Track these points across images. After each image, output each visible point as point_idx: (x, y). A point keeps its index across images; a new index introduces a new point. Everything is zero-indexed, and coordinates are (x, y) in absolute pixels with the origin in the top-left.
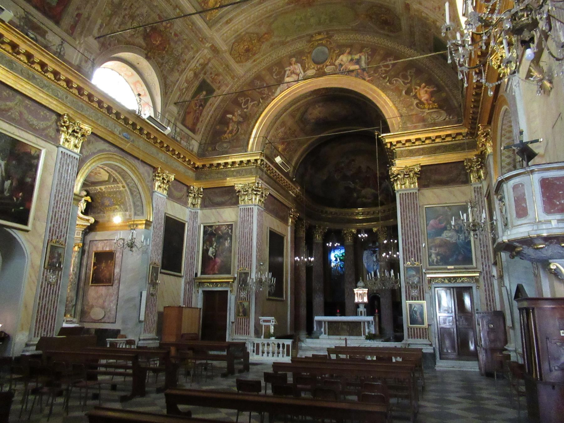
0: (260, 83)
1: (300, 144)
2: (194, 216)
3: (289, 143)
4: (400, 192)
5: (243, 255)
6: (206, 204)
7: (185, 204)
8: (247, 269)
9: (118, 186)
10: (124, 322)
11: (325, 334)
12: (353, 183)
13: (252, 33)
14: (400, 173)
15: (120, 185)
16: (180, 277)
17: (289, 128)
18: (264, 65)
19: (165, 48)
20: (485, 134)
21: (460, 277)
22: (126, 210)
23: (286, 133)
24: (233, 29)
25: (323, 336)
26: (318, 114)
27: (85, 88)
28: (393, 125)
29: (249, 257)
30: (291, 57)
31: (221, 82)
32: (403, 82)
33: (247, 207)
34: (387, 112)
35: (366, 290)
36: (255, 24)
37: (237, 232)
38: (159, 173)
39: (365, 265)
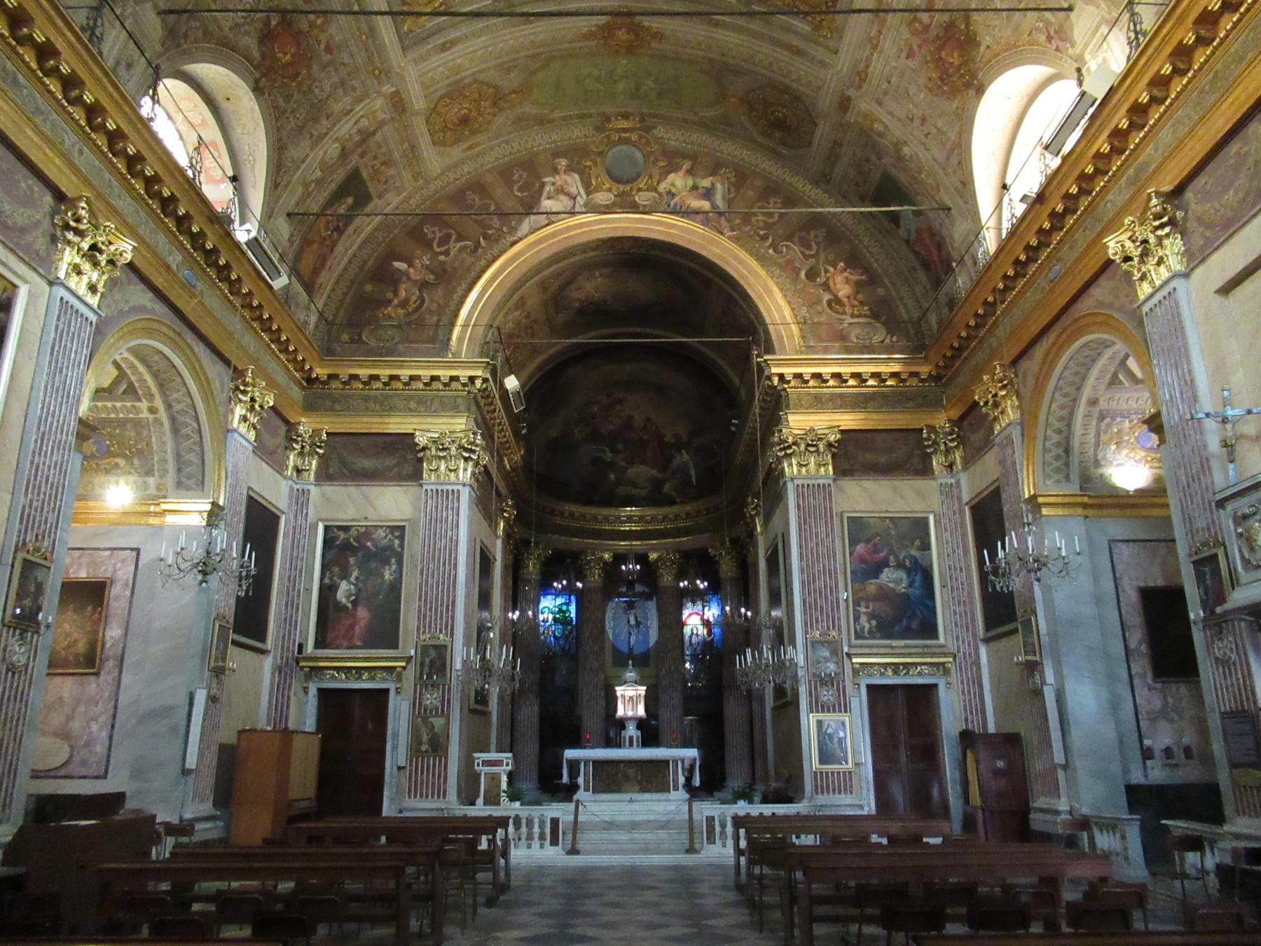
0: (480, 199)
1: (535, 351)
2: (300, 498)
3: (517, 347)
4: (796, 482)
5: (431, 602)
6: (331, 471)
7: (280, 467)
8: (442, 637)
9: (134, 407)
10: (138, 773)
11: (587, 789)
12: (612, 452)
13: (487, 84)
14: (799, 441)
15: (144, 405)
16: (263, 652)
17: (529, 314)
18: (490, 160)
19: (298, 74)
20: (1005, 382)
21: (915, 665)
22: (149, 473)
23: (518, 324)
24: (450, 64)
25: (674, 795)
26: (593, 291)
27: (132, 138)
28: (780, 338)
29: (448, 606)
30: (557, 154)
31: (391, 181)
32: (802, 252)
33: (445, 488)
34: (769, 311)
35: (642, 690)
36: (501, 65)
37: (414, 547)
38: (246, 385)
39: (610, 633)
